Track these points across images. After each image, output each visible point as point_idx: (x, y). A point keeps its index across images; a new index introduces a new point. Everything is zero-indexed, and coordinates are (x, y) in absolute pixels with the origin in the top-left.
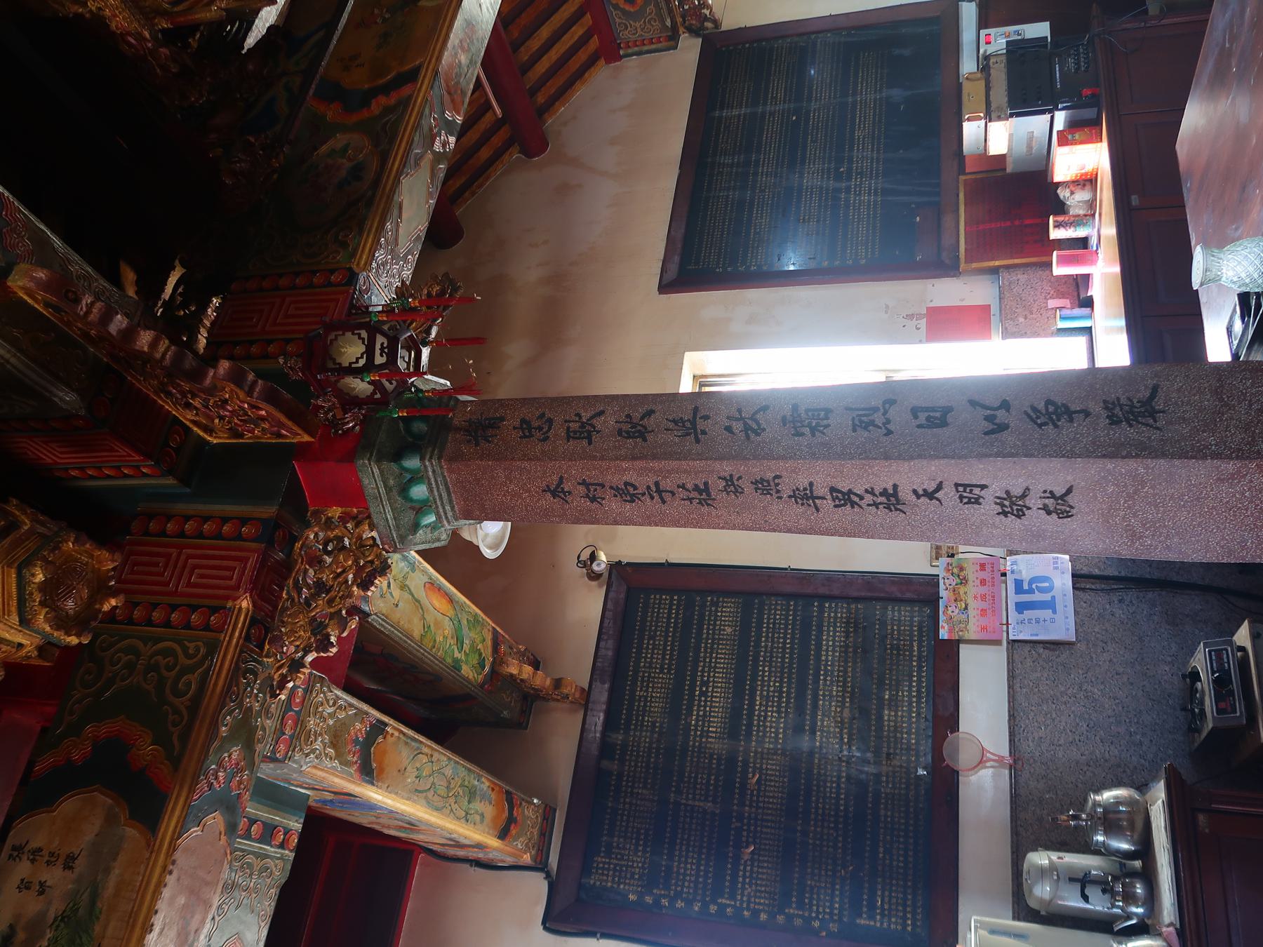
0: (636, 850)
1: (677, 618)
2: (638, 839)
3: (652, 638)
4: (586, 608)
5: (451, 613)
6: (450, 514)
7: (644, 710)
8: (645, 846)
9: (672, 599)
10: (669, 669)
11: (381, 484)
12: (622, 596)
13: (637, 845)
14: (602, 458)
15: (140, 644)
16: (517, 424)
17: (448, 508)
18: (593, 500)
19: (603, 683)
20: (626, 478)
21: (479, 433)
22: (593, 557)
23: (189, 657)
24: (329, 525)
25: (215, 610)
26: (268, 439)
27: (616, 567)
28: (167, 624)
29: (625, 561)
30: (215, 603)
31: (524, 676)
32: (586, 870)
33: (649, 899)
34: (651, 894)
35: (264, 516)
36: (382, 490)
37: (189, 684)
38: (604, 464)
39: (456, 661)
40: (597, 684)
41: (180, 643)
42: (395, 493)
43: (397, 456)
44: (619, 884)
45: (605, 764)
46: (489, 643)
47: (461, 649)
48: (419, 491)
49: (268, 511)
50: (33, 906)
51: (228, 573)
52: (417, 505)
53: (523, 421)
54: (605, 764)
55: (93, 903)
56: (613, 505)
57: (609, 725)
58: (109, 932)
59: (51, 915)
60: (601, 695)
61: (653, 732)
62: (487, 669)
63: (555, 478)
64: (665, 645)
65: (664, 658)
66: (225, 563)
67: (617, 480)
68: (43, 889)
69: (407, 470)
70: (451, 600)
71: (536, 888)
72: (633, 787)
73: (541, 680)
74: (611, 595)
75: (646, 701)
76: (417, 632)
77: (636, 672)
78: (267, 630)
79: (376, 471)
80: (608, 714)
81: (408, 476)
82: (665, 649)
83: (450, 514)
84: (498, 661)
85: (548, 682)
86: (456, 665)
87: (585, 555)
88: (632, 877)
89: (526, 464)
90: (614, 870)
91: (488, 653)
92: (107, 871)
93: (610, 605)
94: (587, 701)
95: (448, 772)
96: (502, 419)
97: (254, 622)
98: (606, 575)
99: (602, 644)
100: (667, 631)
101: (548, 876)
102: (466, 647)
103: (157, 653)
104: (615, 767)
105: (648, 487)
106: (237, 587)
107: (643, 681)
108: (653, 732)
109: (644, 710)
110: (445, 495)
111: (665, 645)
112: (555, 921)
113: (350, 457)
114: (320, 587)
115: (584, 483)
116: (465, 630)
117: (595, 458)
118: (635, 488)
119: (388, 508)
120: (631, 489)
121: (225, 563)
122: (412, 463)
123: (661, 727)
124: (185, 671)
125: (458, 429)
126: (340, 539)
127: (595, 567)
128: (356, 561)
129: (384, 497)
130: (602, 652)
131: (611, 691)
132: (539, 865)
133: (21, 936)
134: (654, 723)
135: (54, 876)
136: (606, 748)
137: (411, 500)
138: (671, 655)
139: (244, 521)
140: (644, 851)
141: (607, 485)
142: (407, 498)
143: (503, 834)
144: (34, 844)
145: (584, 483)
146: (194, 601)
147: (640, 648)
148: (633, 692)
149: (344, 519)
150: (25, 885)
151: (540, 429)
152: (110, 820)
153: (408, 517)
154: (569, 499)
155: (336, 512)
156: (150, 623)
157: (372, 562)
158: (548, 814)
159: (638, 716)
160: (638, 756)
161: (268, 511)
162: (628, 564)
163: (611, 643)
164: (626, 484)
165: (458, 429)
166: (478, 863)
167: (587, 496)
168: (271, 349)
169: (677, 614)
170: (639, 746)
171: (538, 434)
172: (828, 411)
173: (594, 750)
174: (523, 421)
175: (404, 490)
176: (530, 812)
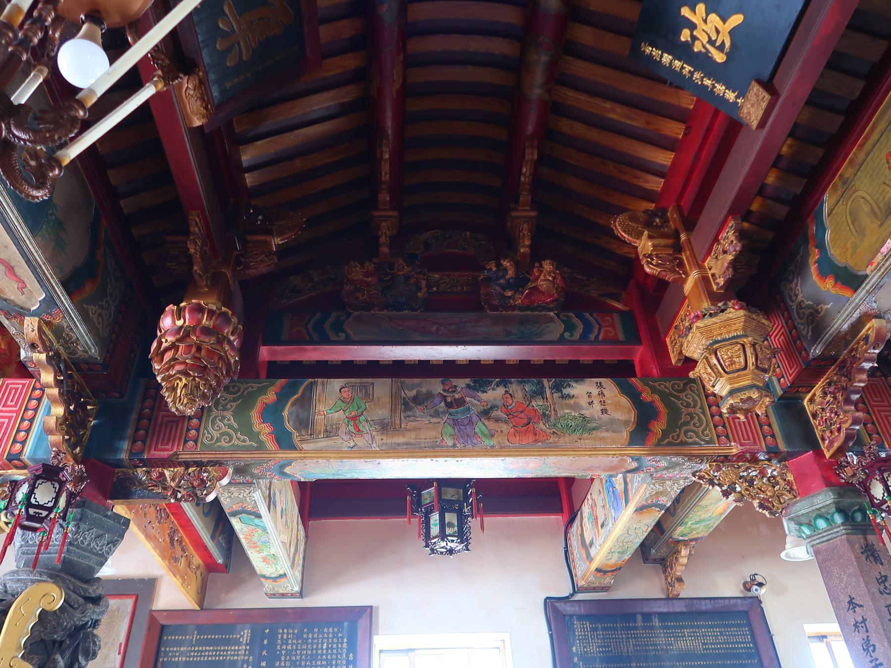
0: (599, 647)
1: (739, 648)
2: (605, 647)
3: (721, 634)
4: (725, 585)
5: (714, 515)
6: (815, 543)
7: (677, 637)
8: (603, 652)
9: (749, 643)
10: (706, 649)
11: (821, 505)
12: (741, 609)
13: (602, 647)
14: (884, 630)
15: (699, 406)
16: (883, 574)
17: (818, 541)
18: (856, 626)
19: (686, 606)
20: (877, 645)
21: (869, 553)
22: (760, 585)
23: (703, 432)
24: (783, 476)
25: (727, 437)
26: (818, 434)
27: (757, 601)
28: (712, 416)
29: (762, 605)
30: (731, 437)
31: (681, 560)
32: (581, 617)
33: (576, 660)
34: (579, 660)
35: (780, 446)
36: (818, 507)
37: (691, 438)
38: (881, 631)
39: (686, 524)
40: (682, 603)
41: (707, 425)
42: (817, 512)
43: (839, 510)
44: (579, 639)
45: (639, 617)
46: (696, 536)
47: (693, 524)
48: (821, 524)
49: (782, 447)
50: (584, 402)
51: (746, 437)
52: (813, 523)
53: (886, 577)
54: (639, 617)
55: (594, 429)
56: (858, 638)
57: (663, 616)
58: (587, 441)
59: (583, 412)
60: (678, 607)
61: (666, 645)
62: (681, 538)
63: (861, 603)
64: (720, 644)
65: (711, 644)
66: (750, 434)
67: (874, 640)
68: (591, 403)
69: (832, 516)
70: (721, 514)
71: (564, 590)
72: (632, 638)
73: (679, 570)
74: (739, 601)
75: (683, 637)
76: (703, 503)
77: (697, 627)
78: (722, 462)
79: (829, 502)
80: (668, 613)
81: (829, 517)
82: (717, 644)
83: (815, 543)
84: (686, 543)
85: (679, 574)
86: (681, 524)
87: (759, 579)
88: (585, 647)
89: (863, 585)
90: (585, 635)
91: (691, 536)
92: (607, 430)
93: (732, 601)
94: (672, 599)
95: (636, 541)
96: (882, 564)
97: (726, 457)
98: (749, 594)
99: (707, 601)
100: (728, 643)
101: (572, 595)
102: (694, 526)
103: (698, 415)
104: (640, 624)
105: (877, 659)
106: (741, 445)
107: (693, 632)
108: (666, 645)
109: (677, 637)
110: (825, 539)
111: (720, 644)
112: (552, 605)
113: (829, 484)
114: (751, 482)
115: (864, 620)
116: (704, 524)
117: (883, 625)
118: (874, 651)
119: (808, 511)
120: (871, 648)
121: (750, 434)
122: (838, 519)
123: (671, 650)
124: (696, 433)
125: (866, 539)
126: (778, 484)
127: (755, 587)
128: (771, 497)
129: (814, 508)
130: (703, 602)
131: (682, 613)
132: (576, 590)
133: (572, 402)
134: (671, 644)
135: (597, 407)
136: (647, 617)
137: (815, 521)
138: (715, 649)
139: (773, 436)
140: (600, 652)
141: (868, 634)
142: (815, 519)
143: (598, 570)
144: (605, 391)
145: (864, 620)
146: (727, 425)
147: (712, 626)
148: (685, 627)
149: (789, 483)
150: (589, 395)
151: (886, 588)
152: (626, 423)
153: (804, 520)
154: (851, 611)
155: (790, 477)
156: (710, 407)
157: (773, 506)
158: (605, 589)
159: (672, 633)
160: (650, 638)
161: (782, 447)
162: (762, 609)
163: (709, 607)
164: (874, 646)
165: (866, 539)
166: (566, 552)
167: (857, 622)
168: (874, 436)
169: (742, 648)
170: (656, 637)
171: (882, 588)
172: (384, 427)
173: (646, 609)
174: (886, 577)
175: (821, 516)
176: (608, 580)
